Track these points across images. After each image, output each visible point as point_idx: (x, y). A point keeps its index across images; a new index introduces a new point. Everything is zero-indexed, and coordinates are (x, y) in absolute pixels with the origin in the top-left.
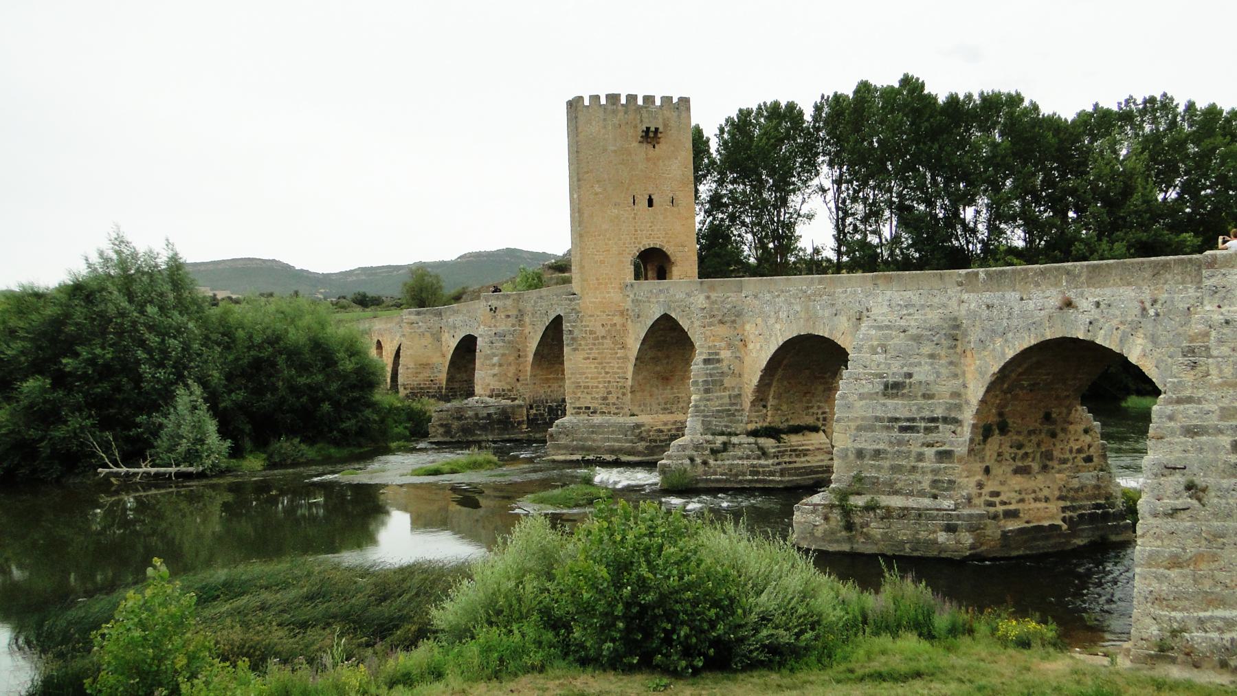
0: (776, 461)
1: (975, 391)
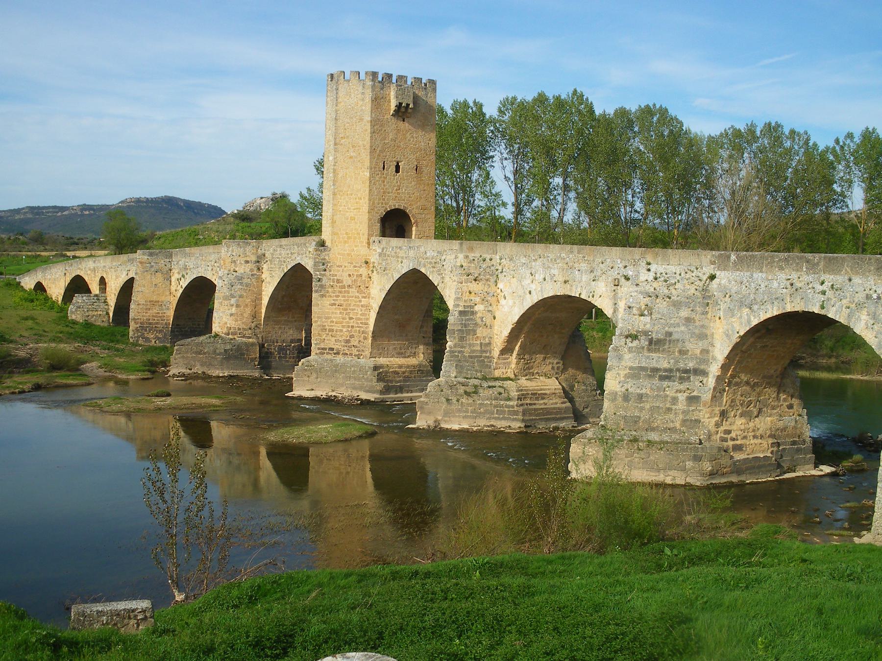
1: (721, 351)
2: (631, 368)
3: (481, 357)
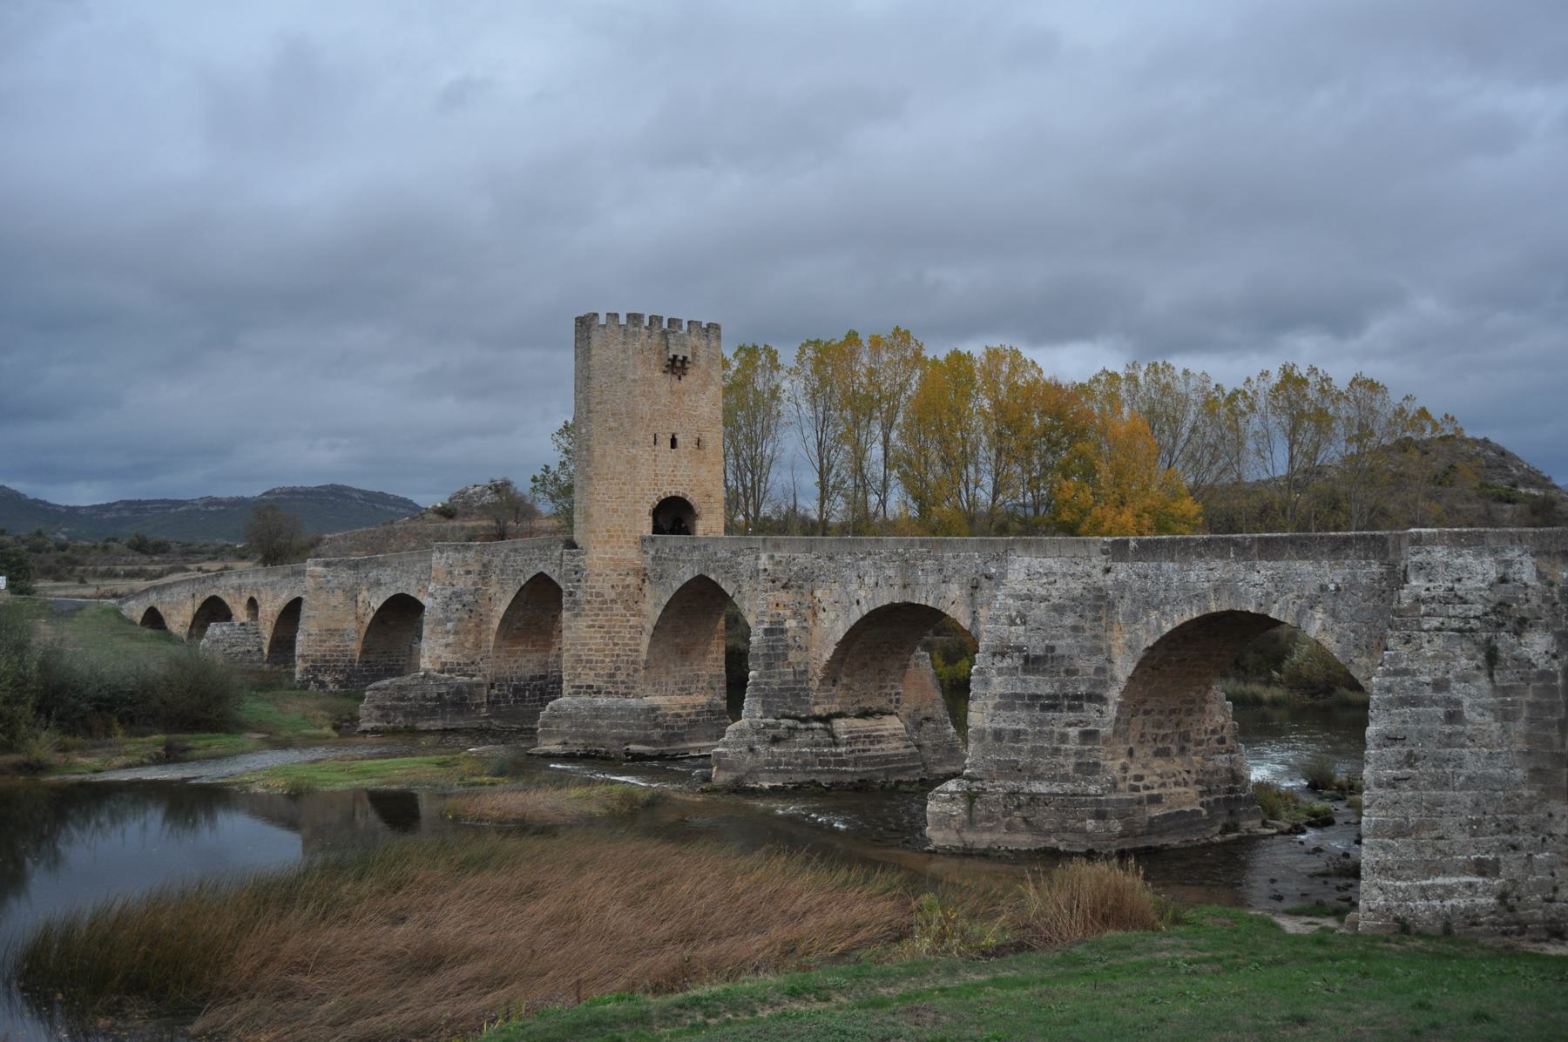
1: (1123, 668)
2: (1002, 696)
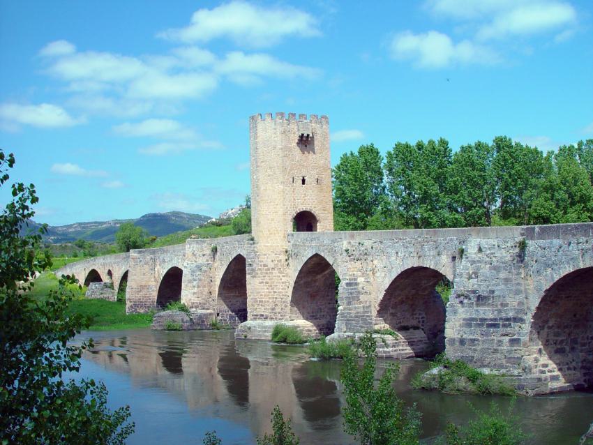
0: (394, 349)
2: (464, 319)
3: (363, 316)
